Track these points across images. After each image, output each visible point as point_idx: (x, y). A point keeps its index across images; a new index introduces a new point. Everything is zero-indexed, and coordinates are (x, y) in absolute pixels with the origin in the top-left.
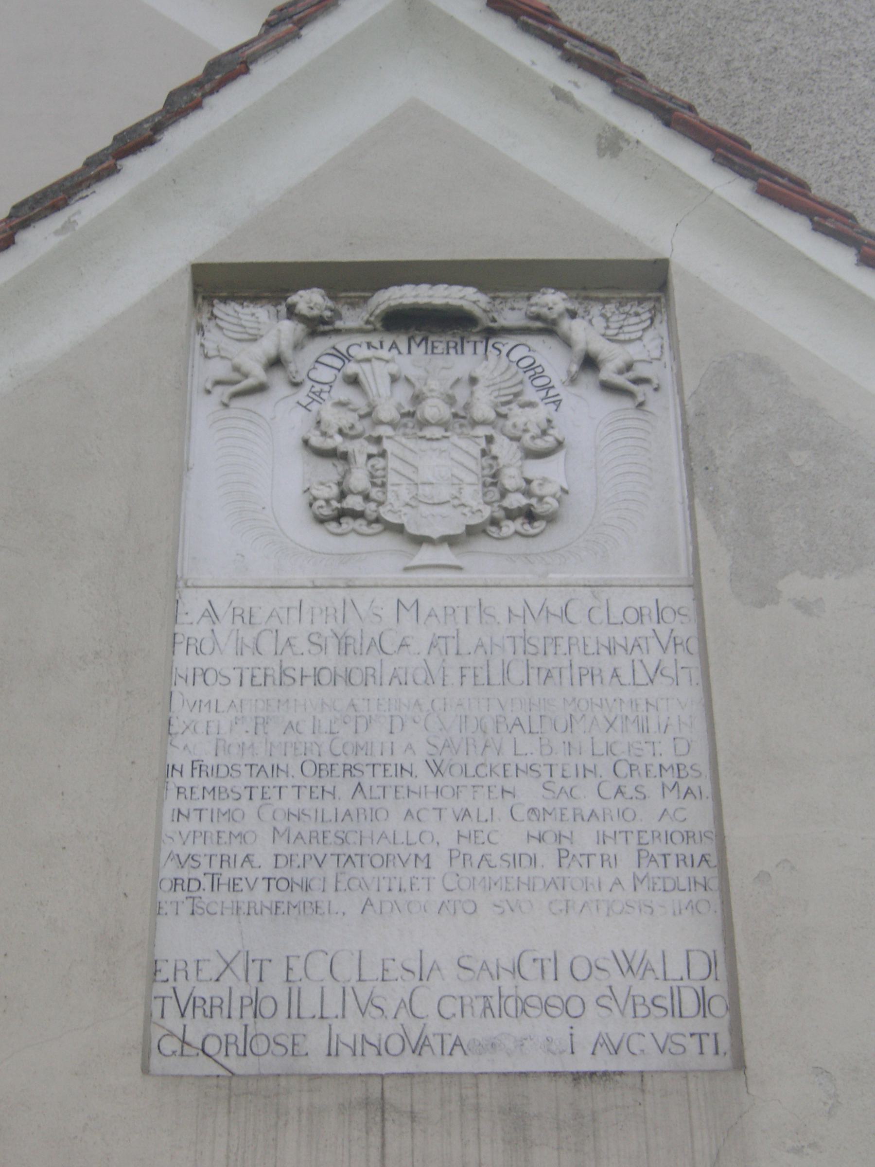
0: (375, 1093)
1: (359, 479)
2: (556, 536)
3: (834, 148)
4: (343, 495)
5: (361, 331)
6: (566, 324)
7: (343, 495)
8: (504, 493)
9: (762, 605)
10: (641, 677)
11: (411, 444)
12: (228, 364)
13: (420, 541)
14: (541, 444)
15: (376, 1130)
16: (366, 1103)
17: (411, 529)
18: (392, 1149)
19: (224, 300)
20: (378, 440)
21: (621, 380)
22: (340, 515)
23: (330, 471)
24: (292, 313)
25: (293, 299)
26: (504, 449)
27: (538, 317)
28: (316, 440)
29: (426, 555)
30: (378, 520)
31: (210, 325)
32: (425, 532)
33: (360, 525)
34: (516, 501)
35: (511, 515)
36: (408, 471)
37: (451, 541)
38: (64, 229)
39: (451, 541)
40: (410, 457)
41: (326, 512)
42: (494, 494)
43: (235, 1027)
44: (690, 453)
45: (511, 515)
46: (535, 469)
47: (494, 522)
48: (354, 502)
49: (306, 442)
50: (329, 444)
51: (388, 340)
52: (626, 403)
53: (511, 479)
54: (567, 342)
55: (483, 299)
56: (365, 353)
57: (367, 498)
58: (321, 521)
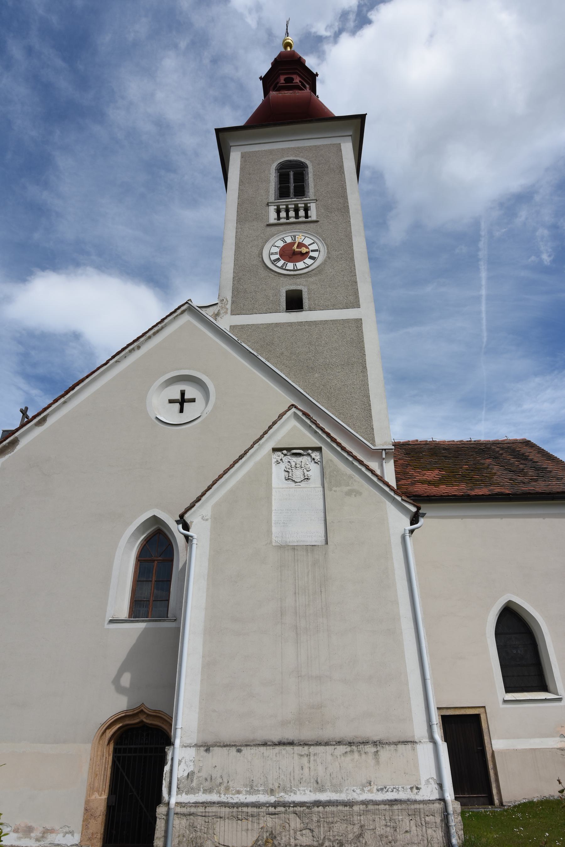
0: (294, 547)
1: (290, 475)
2: (310, 481)
3: (270, 835)
4: (289, 477)
5: (289, 455)
6: (311, 454)
7: (289, 477)
8: (305, 476)
9: (331, 491)
10: (319, 499)
11: (295, 470)
12: (276, 460)
13: (296, 482)
14: (309, 470)
15: (294, 551)
16: (293, 548)
17: (296, 481)
18: (295, 553)
19: (275, 451)
20: (292, 470)
21: (317, 461)
22: (288, 479)
23: (287, 473)
24: (282, 453)
25: (283, 452)
26: (305, 471)
27: (308, 453)
28: (286, 470)
29: (297, 484)
30: (292, 479)
31: (274, 454)
32: (297, 481)
33: (290, 480)
34: (306, 477)
35: (306, 479)
36: (295, 474)
37: (300, 482)
38: (258, 445)
39: (300, 482)
40: (295, 472)
41: (287, 479)
42: (304, 476)
43: (280, 539)
44: (275, 813)
45: (306, 479)
46: (308, 473)
47: (304, 480)
48: (290, 478)
49: (285, 470)
50: (287, 470)
51: (293, 456)
52: (317, 464)
53: (306, 475)
54: (311, 457)
55: (302, 451)
56: (291, 458)
57: (291, 477)
58: (286, 480)
